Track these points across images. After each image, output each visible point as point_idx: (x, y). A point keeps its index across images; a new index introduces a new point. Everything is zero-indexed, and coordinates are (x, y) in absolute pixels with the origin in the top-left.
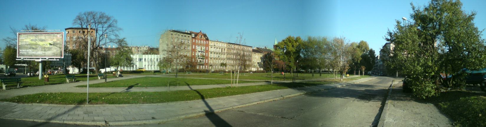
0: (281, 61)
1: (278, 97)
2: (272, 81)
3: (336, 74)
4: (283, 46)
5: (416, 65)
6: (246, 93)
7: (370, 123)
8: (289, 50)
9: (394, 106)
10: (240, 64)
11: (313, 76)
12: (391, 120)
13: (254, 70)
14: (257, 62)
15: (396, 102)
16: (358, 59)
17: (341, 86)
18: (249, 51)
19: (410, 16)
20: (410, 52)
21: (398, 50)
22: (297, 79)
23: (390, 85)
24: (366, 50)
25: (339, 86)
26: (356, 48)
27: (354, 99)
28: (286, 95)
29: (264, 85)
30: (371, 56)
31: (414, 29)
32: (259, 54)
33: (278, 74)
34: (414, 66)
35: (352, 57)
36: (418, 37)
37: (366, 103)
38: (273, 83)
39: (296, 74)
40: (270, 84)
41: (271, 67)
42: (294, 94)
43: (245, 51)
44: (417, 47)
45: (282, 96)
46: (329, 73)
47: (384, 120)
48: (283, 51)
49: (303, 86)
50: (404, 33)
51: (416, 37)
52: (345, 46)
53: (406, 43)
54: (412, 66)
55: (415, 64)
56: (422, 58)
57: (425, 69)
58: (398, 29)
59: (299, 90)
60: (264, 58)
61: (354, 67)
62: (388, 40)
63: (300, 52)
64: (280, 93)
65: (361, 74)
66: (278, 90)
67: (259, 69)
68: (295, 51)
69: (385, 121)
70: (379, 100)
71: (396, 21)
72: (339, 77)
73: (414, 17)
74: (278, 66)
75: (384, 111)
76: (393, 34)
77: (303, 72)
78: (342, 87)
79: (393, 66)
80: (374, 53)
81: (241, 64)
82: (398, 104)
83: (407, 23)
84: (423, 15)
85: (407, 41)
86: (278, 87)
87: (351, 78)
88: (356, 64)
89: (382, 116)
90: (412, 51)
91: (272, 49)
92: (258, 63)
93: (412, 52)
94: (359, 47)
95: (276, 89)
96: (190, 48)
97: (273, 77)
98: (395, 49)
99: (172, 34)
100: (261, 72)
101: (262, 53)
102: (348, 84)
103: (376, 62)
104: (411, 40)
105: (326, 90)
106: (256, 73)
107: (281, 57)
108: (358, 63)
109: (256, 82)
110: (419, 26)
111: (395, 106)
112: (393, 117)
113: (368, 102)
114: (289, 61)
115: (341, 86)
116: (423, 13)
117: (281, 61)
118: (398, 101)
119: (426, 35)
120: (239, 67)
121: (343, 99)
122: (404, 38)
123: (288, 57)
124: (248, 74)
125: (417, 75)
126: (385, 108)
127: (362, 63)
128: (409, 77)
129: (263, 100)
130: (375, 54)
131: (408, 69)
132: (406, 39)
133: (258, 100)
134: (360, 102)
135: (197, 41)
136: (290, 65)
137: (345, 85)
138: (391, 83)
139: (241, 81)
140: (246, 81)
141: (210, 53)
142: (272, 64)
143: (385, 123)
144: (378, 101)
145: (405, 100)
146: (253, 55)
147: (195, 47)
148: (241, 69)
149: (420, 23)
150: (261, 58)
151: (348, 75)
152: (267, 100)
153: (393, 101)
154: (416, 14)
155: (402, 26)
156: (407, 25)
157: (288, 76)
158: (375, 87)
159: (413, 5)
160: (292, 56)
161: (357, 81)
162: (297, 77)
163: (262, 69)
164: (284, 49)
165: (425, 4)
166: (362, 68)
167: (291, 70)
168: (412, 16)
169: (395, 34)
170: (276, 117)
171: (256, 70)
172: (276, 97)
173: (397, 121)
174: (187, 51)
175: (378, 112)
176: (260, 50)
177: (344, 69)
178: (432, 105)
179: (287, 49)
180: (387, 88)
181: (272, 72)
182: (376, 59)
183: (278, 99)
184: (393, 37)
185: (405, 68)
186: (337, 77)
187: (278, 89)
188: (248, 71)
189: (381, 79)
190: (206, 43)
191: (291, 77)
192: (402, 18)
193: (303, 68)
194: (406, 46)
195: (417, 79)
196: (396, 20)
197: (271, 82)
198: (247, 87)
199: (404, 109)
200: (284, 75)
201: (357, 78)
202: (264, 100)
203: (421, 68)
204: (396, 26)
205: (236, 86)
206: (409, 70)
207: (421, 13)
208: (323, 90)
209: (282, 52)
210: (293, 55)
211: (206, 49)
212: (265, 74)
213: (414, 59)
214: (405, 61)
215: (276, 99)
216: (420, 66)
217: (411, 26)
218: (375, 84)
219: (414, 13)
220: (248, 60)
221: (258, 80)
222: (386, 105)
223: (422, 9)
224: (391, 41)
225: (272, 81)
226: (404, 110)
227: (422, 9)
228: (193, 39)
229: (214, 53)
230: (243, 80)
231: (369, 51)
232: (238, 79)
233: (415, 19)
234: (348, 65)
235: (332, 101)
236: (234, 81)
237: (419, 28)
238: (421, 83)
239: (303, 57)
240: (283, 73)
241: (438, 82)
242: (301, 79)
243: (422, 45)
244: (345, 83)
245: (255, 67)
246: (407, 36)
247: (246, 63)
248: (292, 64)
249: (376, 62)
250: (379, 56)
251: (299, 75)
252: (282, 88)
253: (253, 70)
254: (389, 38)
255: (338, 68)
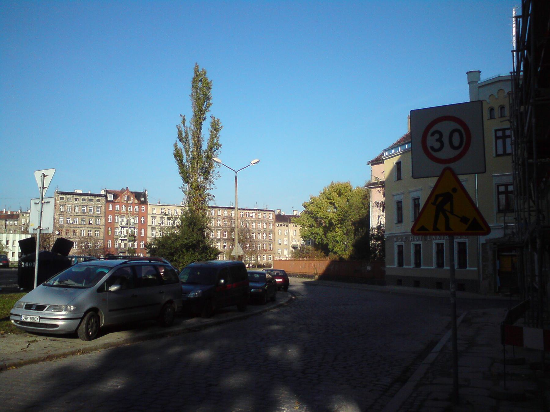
57: (335, 225)
96: (102, 222)
99: (62, 199)
135: (117, 206)
141: (149, 230)
147: (113, 219)
172: (19, 307)
174: (80, 228)
178: (74, 330)
190: (140, 210)
211: (140, 221)
228: (108, 203)
229: (73, 227)
241: (235, 261)
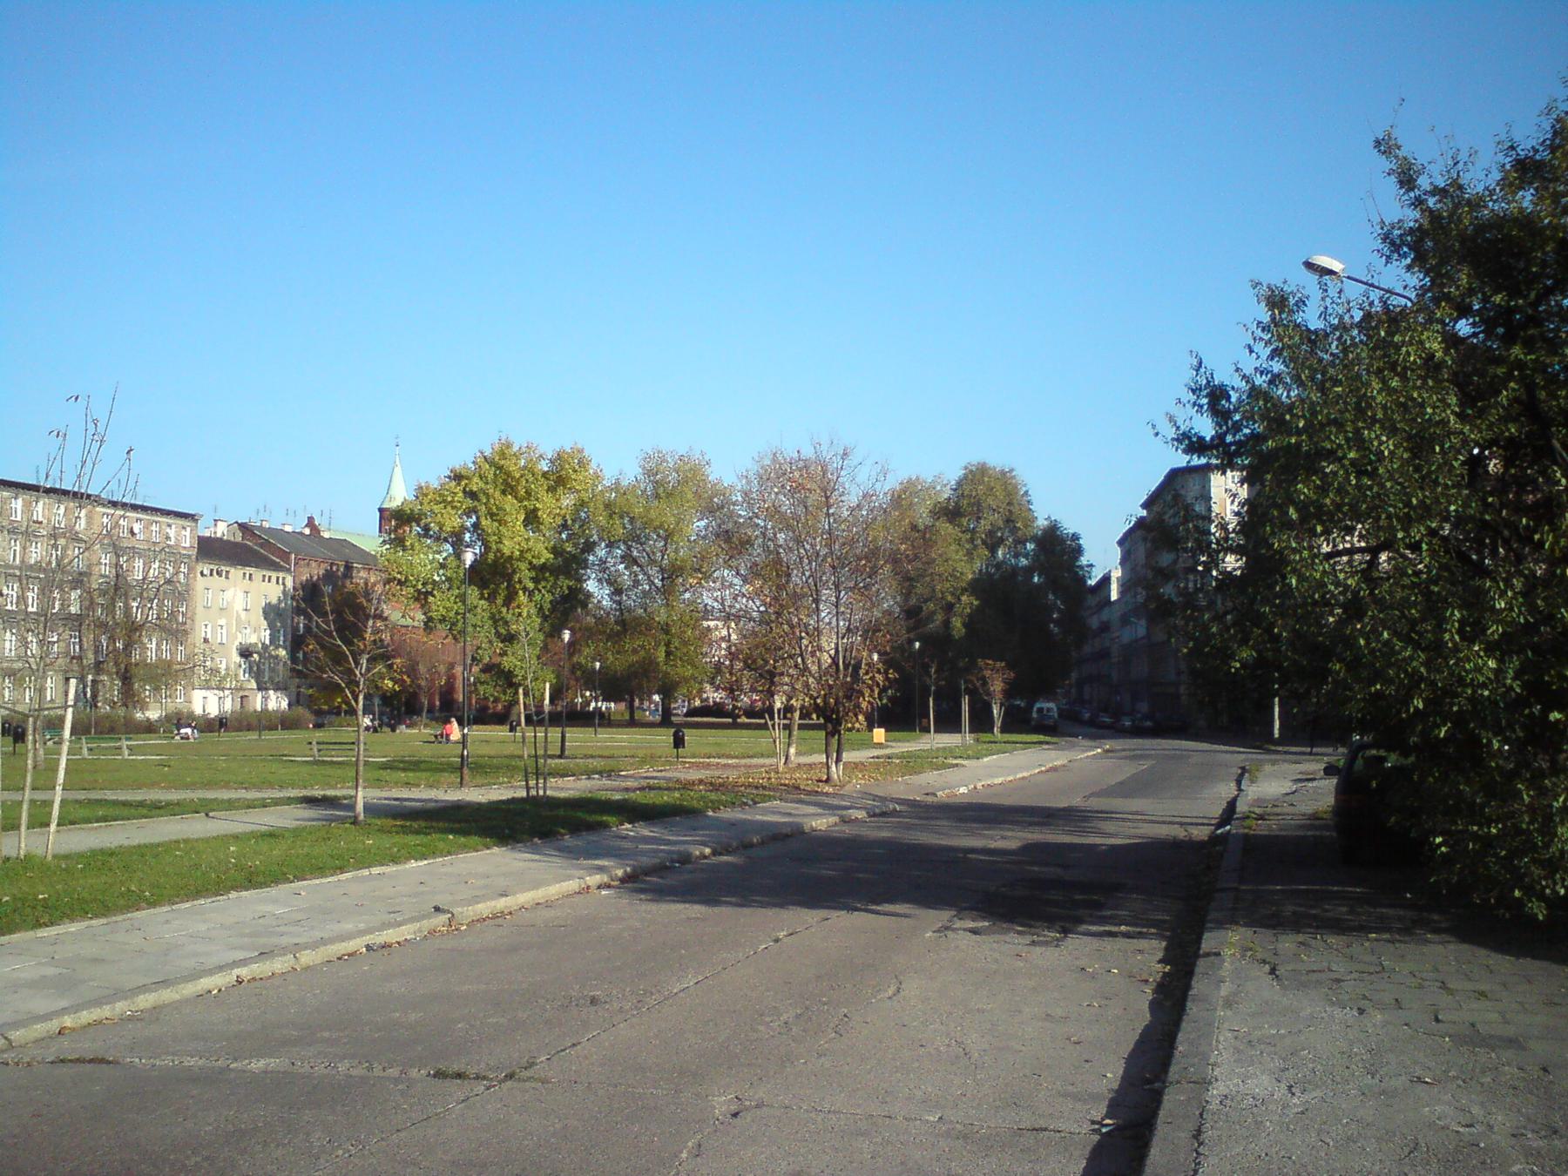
0: (442, 629)
1: (413, 920)
2: (362, 797)
3: (786, 727)
4: (453, 521)
5: (1451, 637)
6: (134, 902)
7: (1095, 1098)
8: (507, 552)
9: (1273, 971)
10: (80, 658)
11: (679, 742)
12: (1265, 1079)
13: (213, 711)
14: (240, 639)
15: (1287, 943)
16: (949, 607)
17: (833, 819)
18: (170, 553)
19: (1378, 244)
20: (1393, 530)
21: (1288, 525)
22: (563, 774)
23: (1217, 811)
24: (1014, 530)
25: (821, 823)
26: (929, 522)
27: (944, 916)
28: (476, 900)
29: (296, 833)
30: (1053, 583)
31: (1421, 342)
32: (258, 574)
33: (414, 737)
34: (1436, 649)
35: (907, 596)
36: (1461, 404)
37: (1046, 944)
38: (369, 808)
39: (555, 733)
40: (342, 820)
41: (353, 683)
42: (536, 885)
43: (134, 552)
44: (1457, 485)
45: (437, 909)
46: (744, 720)
47: (1205, 1083)
48: (458, 555)
49: (606, 826)
50: (1337, 382)
51: (1445, 407)
52: (852, 510)
53: (1353, 462)
54: (1417, 646)
55: (1439, 628)
56: (1507, 582)
58: (1276, 353)
59: (573, 854)
60: (298, 611)
61: (926, 667)
62: (1195, 445)
63: (584, 564)
64: (422, 888)
65: (981, 723)
66: (413, 864)
67: (257, 702)
68: (547, 556)
69: (1216, 1091)
70: (1141, 924)
71: (1264, 291)
72: (811, 752)
73: (1417, 247)
74: (412, 671)
75: (1192, 1008)
76: (1234, 397)
77: (603, 720)
78: (848, 830)
79: (1246, 654)
80: (1079, 551)
81: (90, 658)
82: (1309, 960)
83: (1354, 301)
84: (1499, 222)
85: (1359, 442)
86: (412, 840)
87: (901, 756)
88: (939, 643)
89: (1181, 1047)
90: (1407, 522)
91: (369, 539)
92: (245, 653)
93: (1405, 530)
94: (951, 512)
95: (395, 860)
97: (366, 763)
98: (1255, 515)
100: (272, 728)
101: (276, 567)
102: (883, 799)
103: (1094, 622)
104: (1392, 431)
105: (727, 850)
106: (225, 736)
107: (441, 603)
108: (950, 636)
109: (230, 805)
110: (1464, 311)
111: (1281, 971)
112: (1278, 1063)
113: (1057, 943)
114: (498, 634)
115: (833, 819)
116: (1496, 207)
117: (442, 629)
118: (1301, 937)
119: (1530, 388)
120: (73, 682)
121: (859, 919)
122: (1335, 422)
123: (491, 598)
124: (153, 741)
125: (1459, 721)
126: (1198, 986)
127: (981, 640)
128: (1392, 737)
129: (284, 950)
130: (1084, 561)
131: (1378, 676)
132: (1357, 431)
133: (240, 955)
134: (997, 937)
136: (508, 662)
137: (861, 814)
138: (1227, 790)
139: (90, 802)
140: (141, 804)
142: (364, 662)
143: (1214, 1105)
144: (1140, 935)
145: (1363, 929)
146: (200, 583)
148: (88, 700)
149: (1471, 292)
150: (272, 613)
151: (879, 734)
152: (314, 945)
153: (1265, 935)
154: (1434, 216)
155: (1315, 324)
156: (1358, 315)
157: (485, 750)
158: (1109, 827)
159: (1400, 154)
160: (522, 598)
161: (950, 775)
162: (560, 757)
163: (277, 702)
164: (467, 536)
165: (1509, 126)
166: (987, 673)
167: (517, 702)
168: (1394, 243)
169: (1255, 392)
170: (393, 1072)
171: (228, 706)
173: (1318, 1093)
175: (1147, 1017)
176: (266, 544)
177: (852, 693)
179: (486, 544)
180: (1201, 833)
181: (367, 721)
182: (1092, 601)
183: (406, 932)
184: (1237, 417)
185: (1354, 665)
186: (798, 754)
187: (408, 859)
188: (153, 714)
189: (1141, 757)
191: (513, 757)
192: (1309, 265)
193: (613, 687)
194: (1358, 487)
195: (1469, 751)
196: (1256, 285)
197: (352, 807)
198: (142, 851)
199: (1365, 998)
200: (464, 741)
201: (949, 752)
202: (296, 948)
203: (1500, 661)
204: (1259, 333)
205: (40, 852)
206: (1388, 681)
207: (1476, 203)
208: (707, 851)
209: (443, 566)
210: (531, 585)
212: (304, 743)
213: (1428, 594)
214: (1354, 608)
215: (390, 935)
216: (1490, 649)
217: (1394, 319)
218: (1095, 803)
219: (1411, 217)
220: (162, 628)
221: (242, 794)
222: (1201, 965)
223: (1482, 175)
224: (1223, 452)
225: (362, 797)
226: (1361, 1011)
227: (1482, 175)
230: (110, 795)
231: (1034, 539)
232: (59, 788)
233: (1420, 260)
234: (876, 657)
235: (781, 935)
236: (25, 807)
237: (1464, 327)
238: (1501, 790)
239: (606, 603)
240: (455, 731)
242: (589, 773)
243: (1493, 466)
244: (866, 794)
245: (215, 681)
246: (1362, 408)
247: (136, 656)
248: (523, 659)
249: (1094, 622)
250: (1117, 574)
251: (577, 737)
252: (441, 845)
253: (198, 711)
254: (1206, 427)
255: (807, 685)
